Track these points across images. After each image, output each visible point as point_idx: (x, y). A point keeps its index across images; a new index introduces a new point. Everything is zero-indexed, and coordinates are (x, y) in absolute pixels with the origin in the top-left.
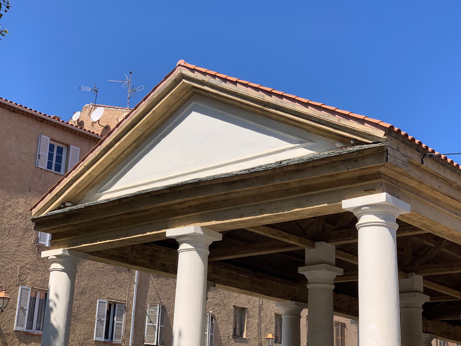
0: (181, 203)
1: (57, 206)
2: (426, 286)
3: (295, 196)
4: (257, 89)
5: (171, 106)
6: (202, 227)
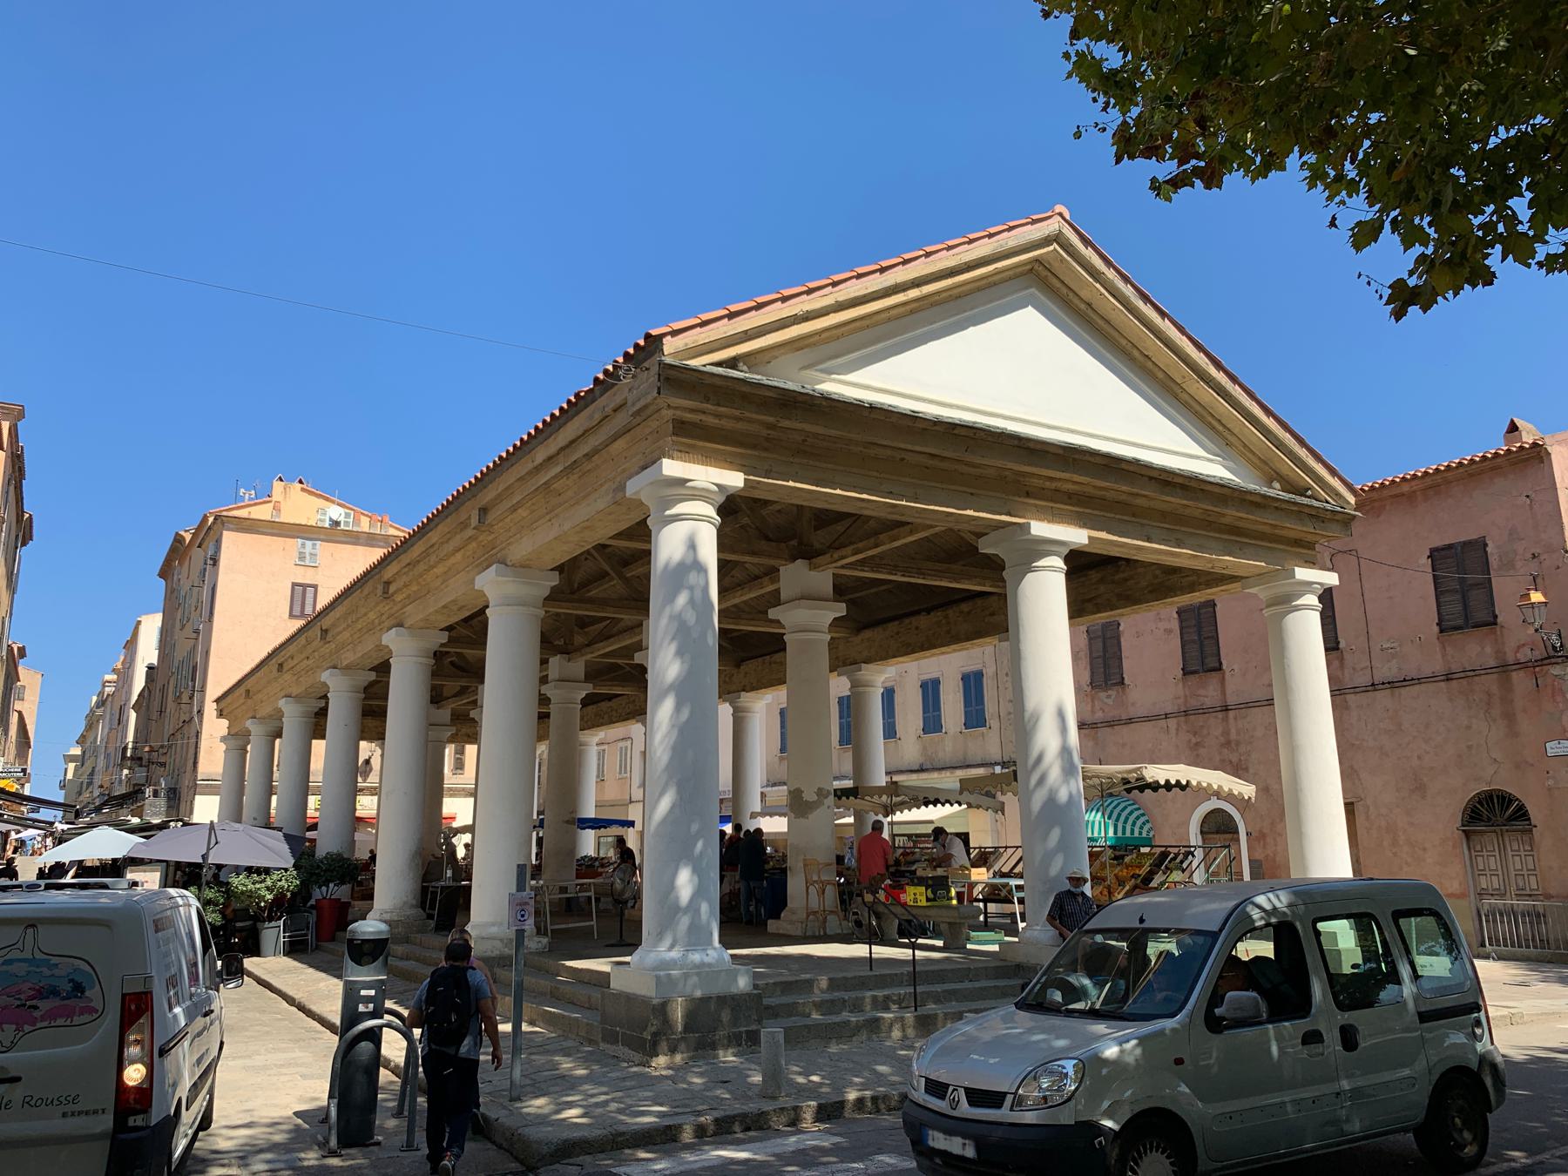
6: (1090, 538)
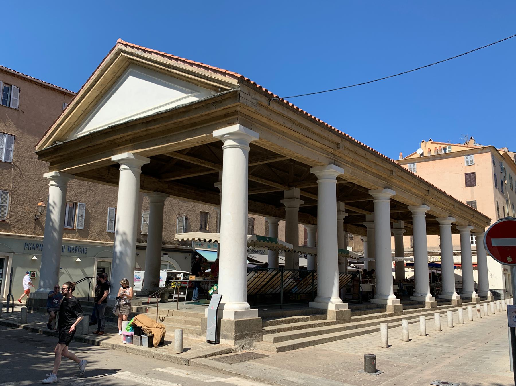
0: (121, 138)
1: (50, 144)
2: (302, 195)
3: (187, 130)
4: (163, 56)
5: (116, 72)
6: (133, 154)
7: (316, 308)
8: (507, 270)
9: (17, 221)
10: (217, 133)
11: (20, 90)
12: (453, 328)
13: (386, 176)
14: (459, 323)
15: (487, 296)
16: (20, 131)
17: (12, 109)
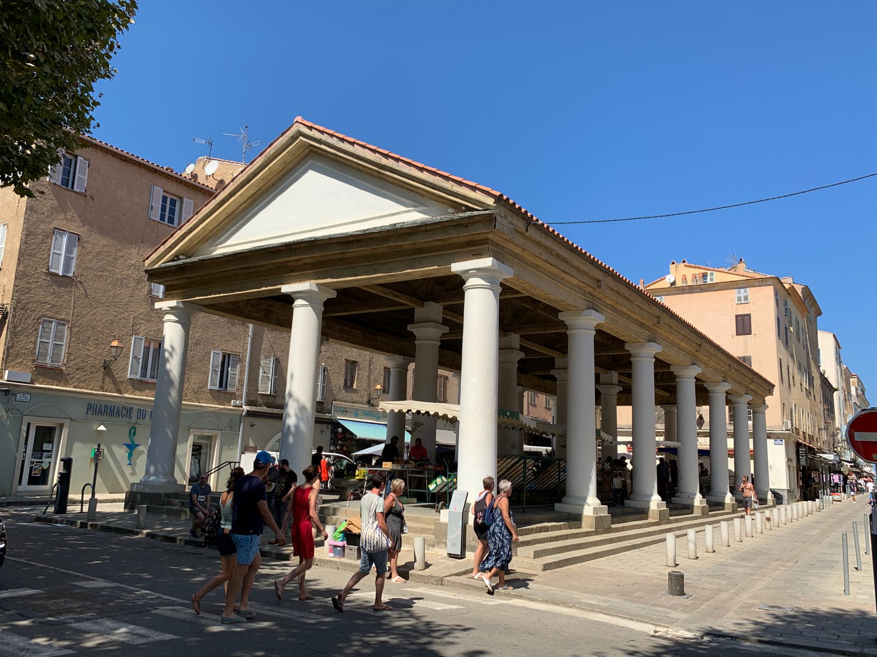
0: (298, 260)
1: (170, 259)
3: (408, 258)
6: (317, 284)
7: (565, 512)
8: (791, 461)
9: (77, 370)
10: (457, 267)
11: (89, 165)
12: (741, 543)
13: (651, 325)
14: (746, 536)
15: (766, 499)
16: (87, 227)
17: (76, 192)
